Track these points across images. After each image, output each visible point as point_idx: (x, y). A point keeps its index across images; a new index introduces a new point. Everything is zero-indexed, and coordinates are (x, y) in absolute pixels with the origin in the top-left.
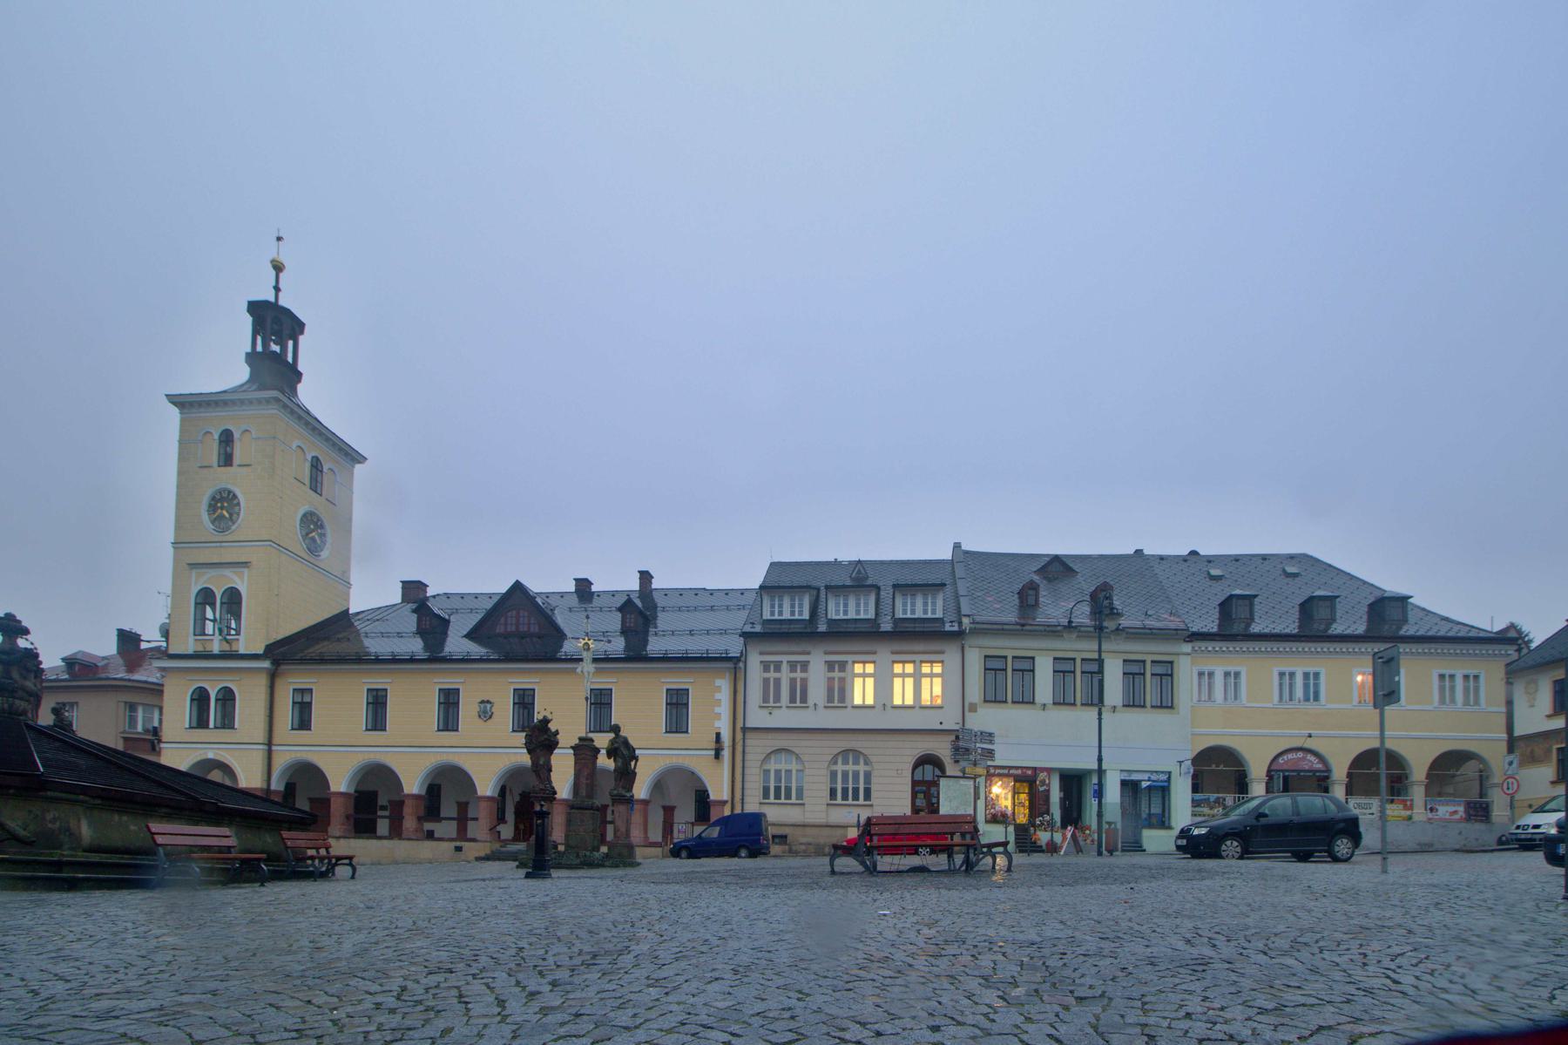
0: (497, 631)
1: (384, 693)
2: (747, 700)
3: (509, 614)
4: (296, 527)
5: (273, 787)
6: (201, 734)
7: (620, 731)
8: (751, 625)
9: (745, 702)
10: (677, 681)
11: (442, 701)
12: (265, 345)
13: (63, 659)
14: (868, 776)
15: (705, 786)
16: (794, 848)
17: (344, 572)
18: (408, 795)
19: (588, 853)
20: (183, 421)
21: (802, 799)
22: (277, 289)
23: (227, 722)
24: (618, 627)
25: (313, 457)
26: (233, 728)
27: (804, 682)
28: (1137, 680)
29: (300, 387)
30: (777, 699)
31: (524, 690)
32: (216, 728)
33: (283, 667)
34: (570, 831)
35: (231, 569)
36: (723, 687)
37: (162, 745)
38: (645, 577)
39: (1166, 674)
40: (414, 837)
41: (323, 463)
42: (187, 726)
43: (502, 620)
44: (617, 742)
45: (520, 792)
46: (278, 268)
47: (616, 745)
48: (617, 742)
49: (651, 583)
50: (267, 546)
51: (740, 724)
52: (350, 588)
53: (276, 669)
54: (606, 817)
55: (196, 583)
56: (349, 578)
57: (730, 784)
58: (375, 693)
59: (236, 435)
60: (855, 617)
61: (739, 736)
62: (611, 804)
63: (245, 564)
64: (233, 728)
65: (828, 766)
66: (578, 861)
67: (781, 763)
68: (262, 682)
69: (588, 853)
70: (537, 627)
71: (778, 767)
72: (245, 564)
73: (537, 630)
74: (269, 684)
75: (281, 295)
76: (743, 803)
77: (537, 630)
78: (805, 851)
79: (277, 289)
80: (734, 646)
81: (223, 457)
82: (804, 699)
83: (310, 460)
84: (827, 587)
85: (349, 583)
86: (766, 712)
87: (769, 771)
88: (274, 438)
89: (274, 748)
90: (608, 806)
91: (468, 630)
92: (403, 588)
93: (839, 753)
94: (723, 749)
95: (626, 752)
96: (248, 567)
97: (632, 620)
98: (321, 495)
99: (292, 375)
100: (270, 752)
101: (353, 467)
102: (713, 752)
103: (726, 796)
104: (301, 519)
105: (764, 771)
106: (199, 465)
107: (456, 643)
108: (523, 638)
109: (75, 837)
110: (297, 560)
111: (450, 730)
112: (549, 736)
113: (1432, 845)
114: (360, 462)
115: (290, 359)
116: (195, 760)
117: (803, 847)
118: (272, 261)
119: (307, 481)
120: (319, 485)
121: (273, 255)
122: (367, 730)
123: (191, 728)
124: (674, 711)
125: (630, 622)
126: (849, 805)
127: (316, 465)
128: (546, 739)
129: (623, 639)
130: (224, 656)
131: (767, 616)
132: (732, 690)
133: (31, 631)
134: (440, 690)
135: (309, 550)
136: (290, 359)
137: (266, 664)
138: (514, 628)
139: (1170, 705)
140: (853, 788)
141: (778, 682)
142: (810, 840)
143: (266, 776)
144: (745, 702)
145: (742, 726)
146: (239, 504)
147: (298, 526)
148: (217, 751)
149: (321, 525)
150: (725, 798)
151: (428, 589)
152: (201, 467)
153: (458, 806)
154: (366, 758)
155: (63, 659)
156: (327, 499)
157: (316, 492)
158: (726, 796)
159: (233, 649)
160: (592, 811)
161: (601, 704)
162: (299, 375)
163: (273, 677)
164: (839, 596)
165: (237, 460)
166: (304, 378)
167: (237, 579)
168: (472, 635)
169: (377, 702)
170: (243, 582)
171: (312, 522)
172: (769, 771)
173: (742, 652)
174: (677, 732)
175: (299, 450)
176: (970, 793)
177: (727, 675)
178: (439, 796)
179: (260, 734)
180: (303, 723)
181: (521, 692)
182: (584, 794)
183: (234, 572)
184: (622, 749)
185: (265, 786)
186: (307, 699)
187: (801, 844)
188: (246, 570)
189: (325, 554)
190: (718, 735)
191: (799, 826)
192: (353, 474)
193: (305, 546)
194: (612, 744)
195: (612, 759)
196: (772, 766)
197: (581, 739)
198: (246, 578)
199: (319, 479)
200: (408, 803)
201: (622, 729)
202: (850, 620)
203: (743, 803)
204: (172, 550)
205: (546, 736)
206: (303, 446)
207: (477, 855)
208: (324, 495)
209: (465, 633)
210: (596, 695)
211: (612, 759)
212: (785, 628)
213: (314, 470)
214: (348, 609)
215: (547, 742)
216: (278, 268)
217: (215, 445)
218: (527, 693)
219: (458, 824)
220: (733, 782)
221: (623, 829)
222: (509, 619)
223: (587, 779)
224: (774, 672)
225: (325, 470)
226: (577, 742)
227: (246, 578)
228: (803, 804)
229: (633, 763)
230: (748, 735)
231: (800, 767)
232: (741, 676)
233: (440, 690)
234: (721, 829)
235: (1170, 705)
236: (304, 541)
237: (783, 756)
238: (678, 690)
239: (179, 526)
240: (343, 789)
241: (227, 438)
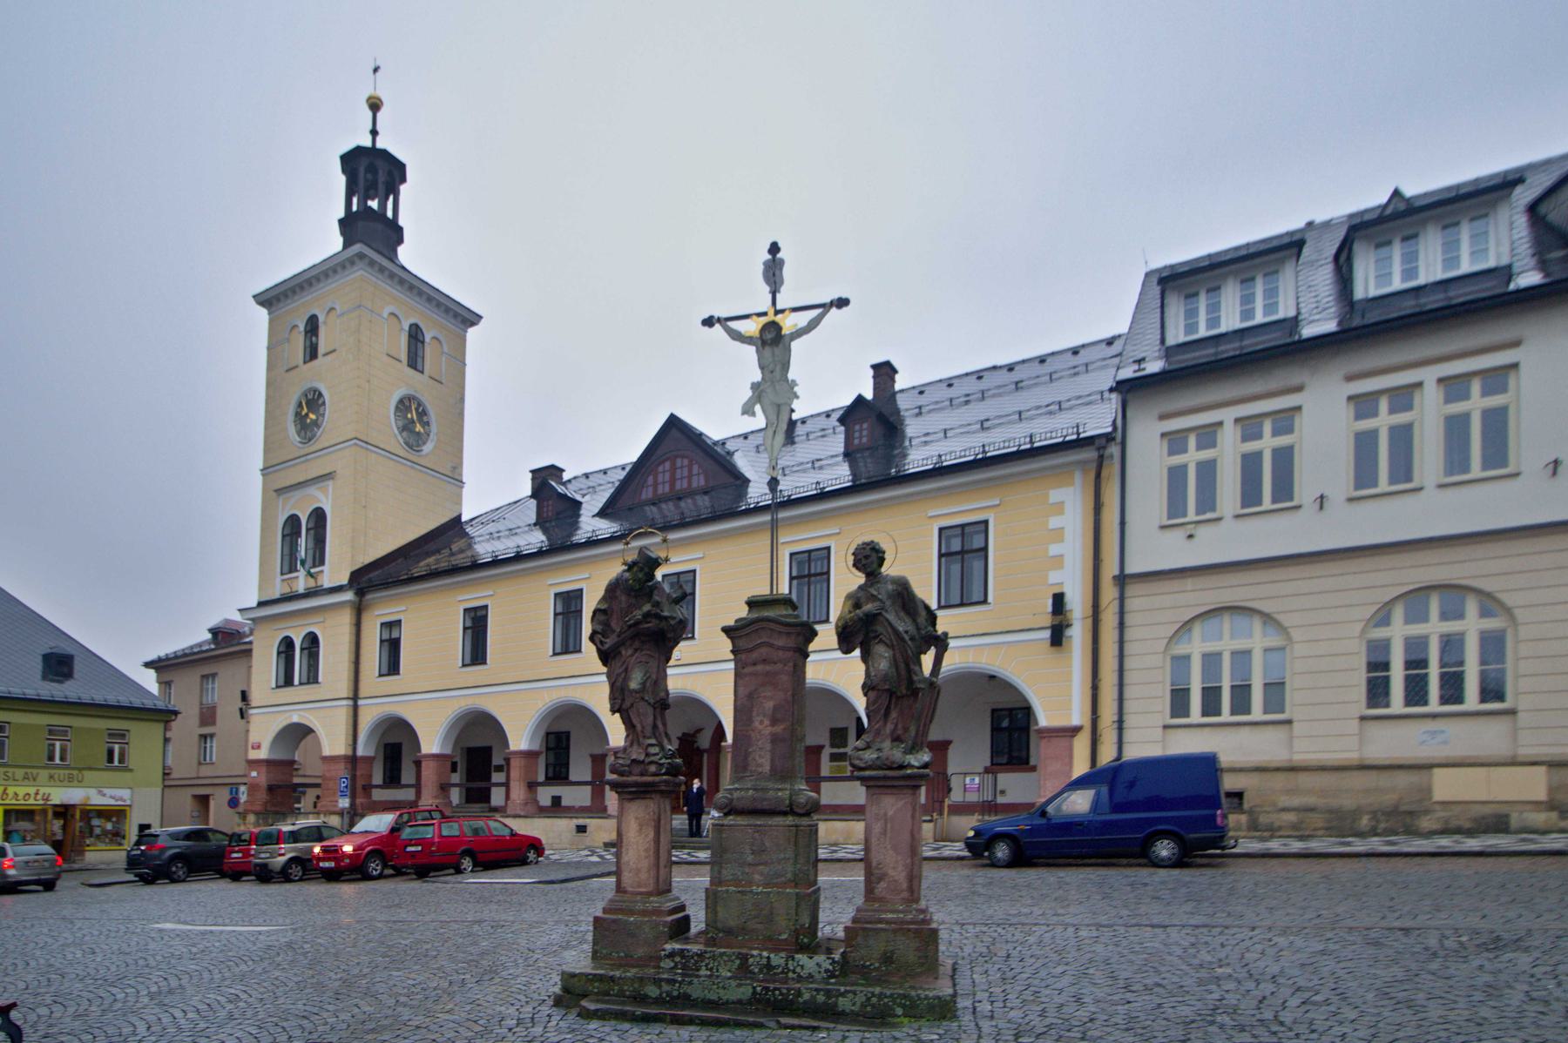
0: (644, 497)
1: (484, 612)
2: (1128, 518)
3: (661, 469)
4: (389, 417)
5: (360, 752)
6: (288, 694)
7: (881, 561)
8: (1136, 367)
9: (1123, 523)
10: (959, 510)
11: (559, 610)
12: (362, 202)
13: (210, 630)
14: (1493, 645)
15: (1026, 700)
16: (1263, 819)
17: (454, 468)
18: (516, 753)
19: (777, 960)
20: (271, 322)
22: (374, 133)
23: (312, 677)
24: (841, 448)
25: (411, 326)
26: (317, 682)
27: (1284, 458)
29: (401, 250)
30: (1207, 501)
31: (678, 574)
32: (301, 684)
33: (369, 597)
34: (720, 883)
35: (317, 486)
36: (1068, 507)
37: (252, 711)
38: (884, 372)
40: (522, 814)
41: (424, 330)
42: (274, 686)
43: (650, 480)
44: (873, 598)
45: (680, 735)
46: (375, 106)
47: (869, 607)
48: (873, 598)
49: (893, 381)
50: (350, 446)
51: (1110, 568)
52: (462, 487)
53: (361, 601)
54: (818, 768)
55: (283, 509)
56: (461, 475)
57: (1089, 693)
58: (472, 614)
59: (321, 319)
60: (1440, 275)
61: (1109, 593)
62: (827, 743)
63: (329, 476)
64: (317, 682)
65: (1363, 631)
66: (744, 992)
67: (1221, 639)
68: (345, 619)
69: (777, 960)
70: (702, 478)
71: (1212, 647)
72: (329, 476)
73: (702, 483)
74: (354, 621)
75: (378, 139)
76: (1120, 729)
77: (702, 483)
78: (1295, 827)
79: (374, 133)
80: (1098, 420)
81: (308, 350)
82: (1284, 488)
83: (407, 328)
85: (461, 482)
86: (1179, 534)
87: (1187, 658)
88: (359, 306)
89: (360, 702)
90: (821, 747)
91: (601, 505)
93: (1397, 598)
94: (1069, 626)
95: (903, 625)
96: (333, 479)
98: (422, 372)
99: (394, 234)
100: (356, 708)
101: (466, 332)
102: (1047, 634)
103: (1077, 715)
104: (397, 408)
105: (1175, 659)
106: (286, 368)
107: (590, 524)
108: (680, 499)
110: (426, 473)
111: (572, 652)
112: (657, 604)
115: (390, 214)
116: (281, 726)
117: (1291, 817)
118: (369, 99)
119: (404, 356)
120: (419, 360)
121: (369, 92)
122: (464, 665)
123: (278, 687)
124: (956, 568)
125: (861, 438)
126: (1434, 716)
127: (415, 335)
128: (647, 615)
129: (847, 464)
130: (309, 594)
131: (1176, 336)
132: (1091, 505)
134: (556, 595)
135: (407, 443)
137: (349, 596)
138: (667, 489)
140: (1443, 676)
141: (1208, 471)
142: (1311, 800)
143: (351, 738)
144: (1123, 523)
145: (1116, 572)
146: (324, 403)
147: (392, 416)
148: (302, 713)
149: (423, 410)
150: (1075, 721)
151: (564, 474)
152: (287, 371)
153: (593, 761)
154: (463, 704)
155: (210, 630)
156: (431, 378)
157: (416, 369)
158: (1077, 715)
159: (319, 584)
160: (790, 820)
161: (810, 575)
162: (399, 231)
163: (359, 610)
164: (1389, 243)
165: (321, 350)
167: (324, 500)
168: (602, 514)
169: (477, 623)
170: (327, 498)
171: (411, 413)
172: (1187, 658)
173: (1114, 423)
174: (962, 605)
175: (393, 317)
177: (1078, 476)
178: (568, 748)
179: (344, 689)
180: (392, 665)
181: (674, 579)
182: (767, 768)
183: (318, 488)
184: (891, 617)
185: (350, 753)
186: (395, 635)
187: (1284, 810)
188: (330, 483)
189: (428, 448)
190: (1059, 600)
191: (1278, 769)
192: (465, 340)
193: (402, 441)
194: (857, 605)
195: (857, 652)
196: (1196, 646)
197: (752, 604)
198: (330, 497)
199: (420, 353)
200: (516, 764)
201: (888, 557)
202: (1425, 286)
203: (1120, 729)
204: (261, 477)
205: (647, 608)
206: (397, 313)
207: (607, 840)
208: (426, 371)
209: (597, 511)
210: (800, 563)
211: (857, 652)
212: (1229, 349)
213: (413, 341)
214: (459, 516)
215: (652, 624)
216: (375, 106)
217: (301, 338)
218: (683, 578)
219: (593, 790)
220: (1095, 688)
221: (899, 874)
222: (660, 479)
223: (774, 722)
225: (427, 339)
226: (743, 612)
227: (330, 497)
228: (1289, 722)
229: (927, 660)
230: (1132, 590)
231: (1275, 641)
232: (1112, 471)
233: (556, 595)
234: (1097, 794)
236: (400, 433)
237: (1226, 621)
238: (963, 526)
239: (267, 451)
240: (435, 750)
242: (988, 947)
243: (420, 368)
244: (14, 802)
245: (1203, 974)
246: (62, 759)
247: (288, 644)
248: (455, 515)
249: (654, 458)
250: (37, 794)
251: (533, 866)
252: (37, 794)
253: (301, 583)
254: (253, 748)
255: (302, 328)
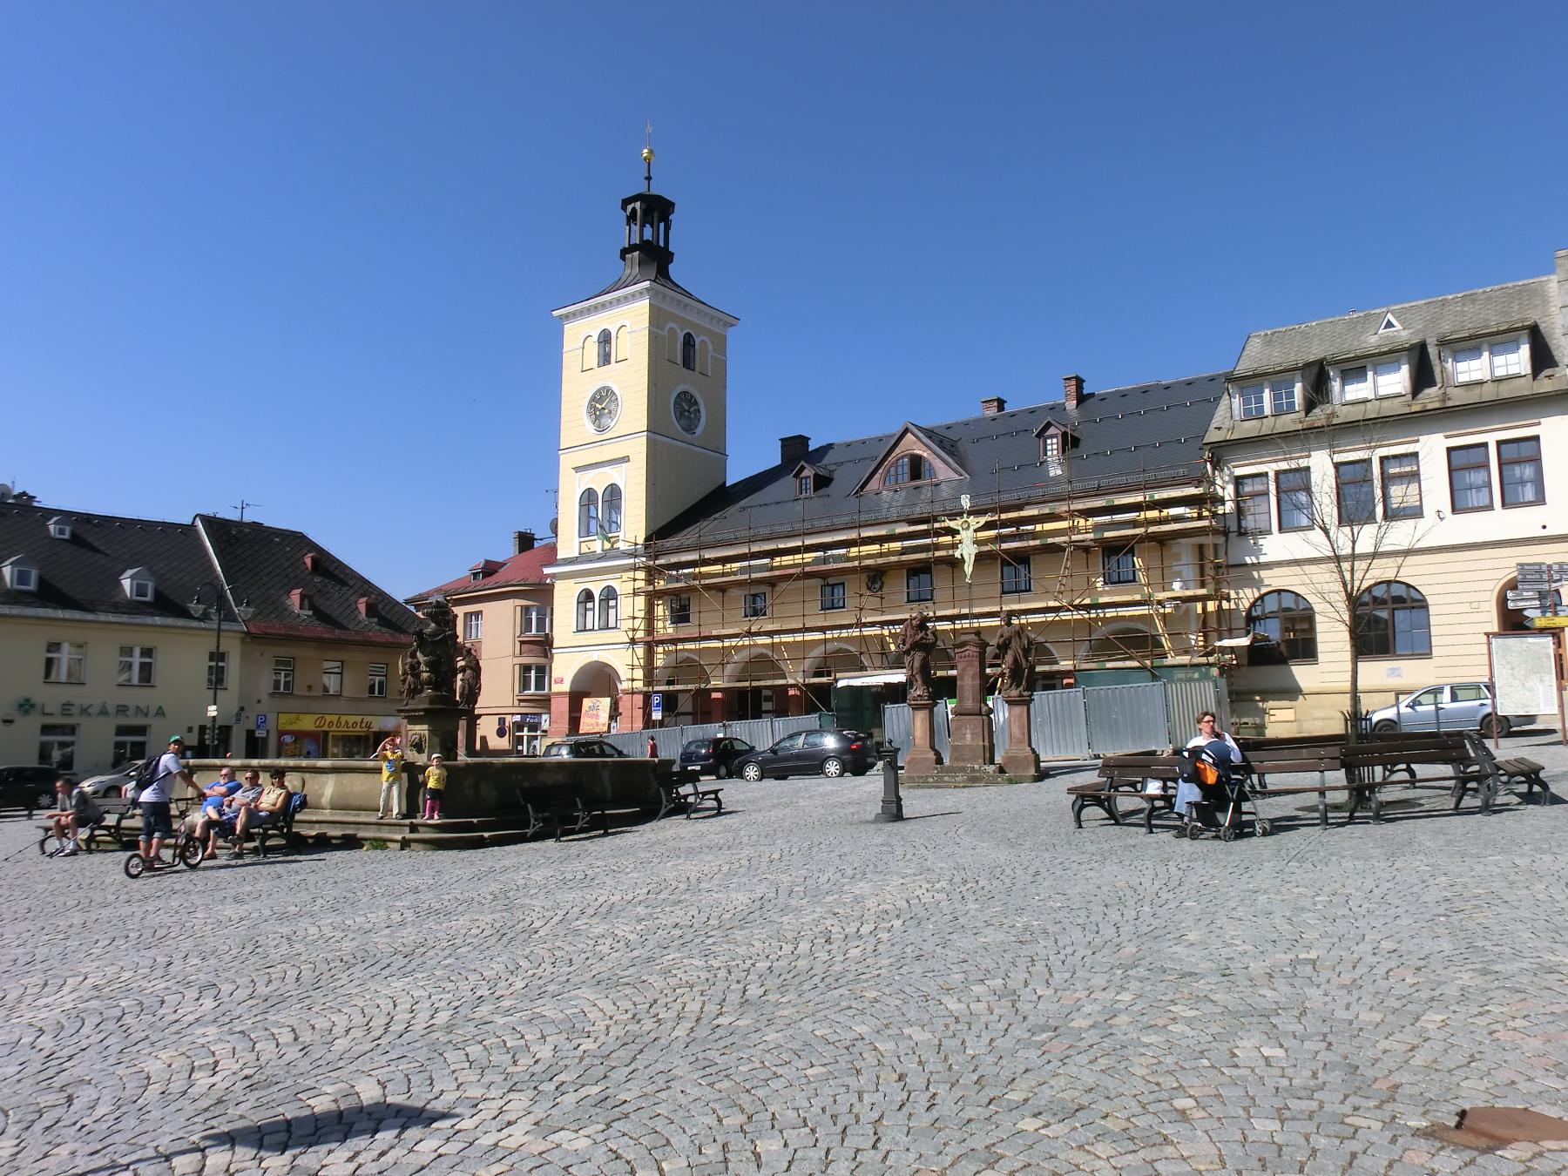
21: (151, 657)
28: (836, 590)
29: (671, 267)
39: (1524, 455)
81: (602, 357)
84: (1443, 343)
92: (783, 447)
97: (1055, 447)
104: (675, 401)
109: (1009, 721)
113: (1531, 719)
114: (732, 325)
115: (662, 244)
123: (578, 631)
130: (605, 556)
133: (39, 728)
136: (662, 244)
139: (1131, 578)
166: (675, 258)
176: (1548, 656)
224: (141, 663)
235: (1131, 578)
241: (605, 338)
242: (809, 1099)
243: (692, 367)
244: (345, 729)
245: (159, 972)
246: (380, 692)
247: (588, 596)
248: (721, 483)
249: (893, 455)
250: (362, 722)
251: (702, 741)
252: (362, 722)
253: (597, 546)
254: (556, 682)
255: (595, 338)
